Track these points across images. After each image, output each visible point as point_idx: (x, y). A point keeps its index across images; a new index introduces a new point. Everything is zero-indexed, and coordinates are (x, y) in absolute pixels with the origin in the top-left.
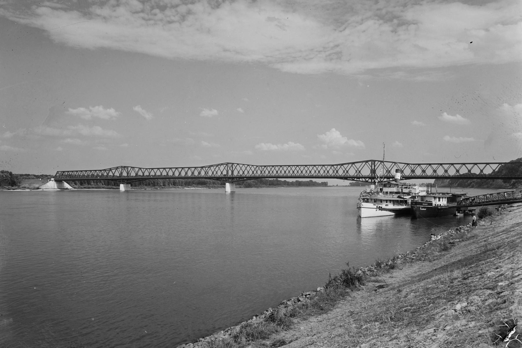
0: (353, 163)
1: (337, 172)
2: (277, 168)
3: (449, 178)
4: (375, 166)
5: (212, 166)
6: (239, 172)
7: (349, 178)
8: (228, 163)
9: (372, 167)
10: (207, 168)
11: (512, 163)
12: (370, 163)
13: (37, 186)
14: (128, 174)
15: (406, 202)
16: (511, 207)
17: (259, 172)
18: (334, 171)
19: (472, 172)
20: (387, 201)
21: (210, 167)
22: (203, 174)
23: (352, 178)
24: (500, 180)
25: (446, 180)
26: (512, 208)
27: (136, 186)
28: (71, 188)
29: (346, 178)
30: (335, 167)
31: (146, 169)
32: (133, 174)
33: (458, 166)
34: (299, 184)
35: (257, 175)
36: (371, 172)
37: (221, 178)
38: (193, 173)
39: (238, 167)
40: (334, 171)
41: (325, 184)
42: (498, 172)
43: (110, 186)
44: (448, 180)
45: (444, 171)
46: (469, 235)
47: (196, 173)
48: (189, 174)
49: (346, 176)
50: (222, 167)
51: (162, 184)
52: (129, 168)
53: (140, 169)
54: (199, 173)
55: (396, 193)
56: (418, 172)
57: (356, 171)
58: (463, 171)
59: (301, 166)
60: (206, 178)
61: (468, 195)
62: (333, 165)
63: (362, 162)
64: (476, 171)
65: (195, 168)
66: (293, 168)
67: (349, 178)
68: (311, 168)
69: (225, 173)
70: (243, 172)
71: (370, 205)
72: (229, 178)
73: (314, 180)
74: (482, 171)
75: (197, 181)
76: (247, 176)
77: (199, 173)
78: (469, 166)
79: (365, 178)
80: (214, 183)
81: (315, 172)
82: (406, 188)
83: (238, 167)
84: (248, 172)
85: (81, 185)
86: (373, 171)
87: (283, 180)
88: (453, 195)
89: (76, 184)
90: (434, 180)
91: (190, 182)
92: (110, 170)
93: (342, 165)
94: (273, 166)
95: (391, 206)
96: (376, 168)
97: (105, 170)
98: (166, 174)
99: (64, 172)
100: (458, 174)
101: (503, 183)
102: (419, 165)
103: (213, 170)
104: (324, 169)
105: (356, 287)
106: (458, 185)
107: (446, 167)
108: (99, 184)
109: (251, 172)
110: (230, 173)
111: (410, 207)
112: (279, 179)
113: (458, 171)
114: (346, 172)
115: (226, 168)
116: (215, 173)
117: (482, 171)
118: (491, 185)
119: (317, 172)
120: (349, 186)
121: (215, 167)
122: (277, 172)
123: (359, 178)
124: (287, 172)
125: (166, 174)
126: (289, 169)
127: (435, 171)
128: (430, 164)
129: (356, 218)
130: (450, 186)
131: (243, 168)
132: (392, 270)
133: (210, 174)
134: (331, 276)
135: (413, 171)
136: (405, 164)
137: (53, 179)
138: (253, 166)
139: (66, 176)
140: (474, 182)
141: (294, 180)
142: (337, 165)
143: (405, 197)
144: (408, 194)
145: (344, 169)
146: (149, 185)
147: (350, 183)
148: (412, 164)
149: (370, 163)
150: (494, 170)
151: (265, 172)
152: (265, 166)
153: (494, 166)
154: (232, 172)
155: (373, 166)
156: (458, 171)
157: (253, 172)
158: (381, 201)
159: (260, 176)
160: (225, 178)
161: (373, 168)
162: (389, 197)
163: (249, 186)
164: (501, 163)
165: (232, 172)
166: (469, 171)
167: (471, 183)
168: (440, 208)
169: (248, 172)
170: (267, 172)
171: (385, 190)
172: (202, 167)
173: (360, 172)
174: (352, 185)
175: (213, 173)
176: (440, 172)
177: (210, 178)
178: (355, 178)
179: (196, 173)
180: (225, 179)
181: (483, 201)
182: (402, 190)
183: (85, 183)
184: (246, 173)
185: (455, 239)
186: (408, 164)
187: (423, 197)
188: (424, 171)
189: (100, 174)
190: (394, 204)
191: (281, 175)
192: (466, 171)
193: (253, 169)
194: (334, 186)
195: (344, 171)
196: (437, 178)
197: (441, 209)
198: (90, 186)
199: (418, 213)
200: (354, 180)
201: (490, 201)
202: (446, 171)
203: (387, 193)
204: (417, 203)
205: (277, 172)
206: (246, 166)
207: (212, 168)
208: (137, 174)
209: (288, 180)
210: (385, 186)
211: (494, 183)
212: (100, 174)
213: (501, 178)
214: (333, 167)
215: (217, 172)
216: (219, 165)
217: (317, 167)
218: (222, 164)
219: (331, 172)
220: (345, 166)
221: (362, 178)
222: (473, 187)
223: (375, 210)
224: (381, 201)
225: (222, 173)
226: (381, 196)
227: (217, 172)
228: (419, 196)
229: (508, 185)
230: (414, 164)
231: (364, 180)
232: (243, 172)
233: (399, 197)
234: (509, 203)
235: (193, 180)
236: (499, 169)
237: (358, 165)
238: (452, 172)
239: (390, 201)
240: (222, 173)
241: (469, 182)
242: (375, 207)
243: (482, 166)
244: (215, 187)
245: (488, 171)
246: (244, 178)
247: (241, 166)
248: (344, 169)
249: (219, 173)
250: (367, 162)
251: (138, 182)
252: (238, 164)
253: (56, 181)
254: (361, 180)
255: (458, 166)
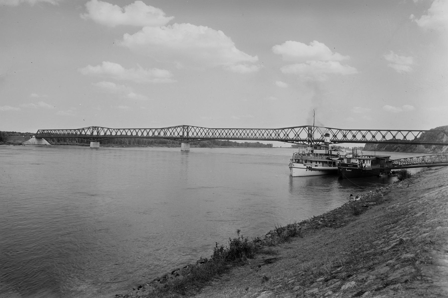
0: (293, 128)
1: (279, 135)
2: (233, 131)
3: (376, 142)
4: (311, 131)
5: (170, 128)
6: (193, 134)
7: (289, 140)
8: (184, 126)
9: (309, 131)
10: (166, 130)
11: (431, 131)
12: (307, 128)
13: (20, 142)
14: (98, 133)
15: (334, 164)
16: (430, 170)
17: (211, 134)
18: (276, 135)
19: (397, 138)
20: (316, 162)
21: (168, 128)
22: (162, 134)
23: (292, 141)
24: (422, 146)
25: (375, 144)
26: (431, 171)
27: (105, 144)
28: (49, 144)
29: (286, 141)
30: (277, 131)
31: (114, 129)
32: (102, 134)
33: (384, 133)
34: (247, 145)
35: (209, 136)
36: (308, 136)
37: (178, 138)
38: (153, 134)
39: (193, 130)
40: (276, 135)
41: (270, 146)
42: (420, 138)
43: (82, 144)
44: (377, 145)
45: (352, 136)
46: (384, 198)
47: (156, 134)
48: (151, 134)
49: (297, 139)
50: (179, 129)
51: (128, 143)
52: (99, 128)
53: (109, 129)
54: (159, 134)
55: (326, 155)
56: (349, 137)
57: (295, 135)
58: (389, 137)
59: (255, 129)
60: (164, 138)
61: (391, 158)
62: (275, 130)
63: (301, 127)
64: (400, 137)
65: (156, 129)
66: (241, 131)
67: (289, 140)
68: (256, 131)
69: (181, 134)
70: (197, 134)
71: (301, 166)
72: (185, 138)
73: (261, 142)
74: (405, 137)
75: (158, 140)
76: (200, 137)
77: (159, 134)
78: (394, 133)
79: (303, 141)
80: (173, 143)
81: (260, 134)
82: (335, 150)
83: (193, 130)
84: (201, 134)
85: (58, 142)
86: (310, 135)
87: (234, 141)
88: (376, 158)
89: (53, 141)
90: (365, 144)
91: (152, 142)
92: (83, 129)
93: (283, 129)
94: (223, 129)
95: (320, 167)
96: (312, 132)
97: (79, 130)
98: (125, 134)
99: (44, 130)
100: (384, 140)
101: (424, 149)
102: (350, 130)
103: (171, 131)
104: (268, 132)
105: (241, 260)
106: (386, 149)
107: (373, 133)
108: (73, 141)
109: (203, 134)
110: (185, 134)
111: (337, 168)
112: (230, 141)
113: (384, 137)
114: (286, 135)
115: (182, 130)
116: (172, 134)
117: (405, 137)
118: (414, 149)
119: (261, 135)
120: (291, 148)
121: (173, 129)
122: (226, 134)
123: (298, 141)
124: (235, 134)
125: (125, 134)
126: (244, 132)
127: (364, 137)
128: (360, 131)
129: (288, 178)
130: (379, 150)
131: (197, 130)
132: (291, 238)
133: (168, 134)
134: (218, 246)
135: (345, 136)
136: (338, 129)
137: (34, 136)
138: (205, 128)
139: (46, 134)
140: (399, 147)
141: (243, 141)
142: (279, 129)
143: (333, 159)
144: (337, 156)
145: (285, 133)
146: (117, 143)
147: (292, 146)
148: (344, 130)
149: (307, 128)
150: (416, 137)
151: (216, 134)
152: (216, 129)
153: (416, 133)
154: (188, 133)
155: (310, 131)
156: (384, 137)
157: (206, 134)
158: (311, 162)
159: (212, 137)
160: (181, 138)
161: (310, 132)
162: (319, 159)
163: (203, 146)
164: (422, 131)
165: (188, 133)
166: (394, 137)
167: (397, 148)
168: (364, 169)
169: (201, 134)
170: (218, 134)
171: (316, 151)
172: (162, 129)
173: (298, 135)
174: (293, 147)
175: (171, 134)
176: (369, 137)
177: (168, 138)
178: (294, 140)
179: (140, 134)
180: (180, 140)
181: (404, 164)
182: (331, 152)
183: (62, 140)
184: (199, 134)
185: (370, 202)
186: (340, 130)
187: (349, 159)
188: (354, 136)
189: (74, 133)
190: (323, 165)
191: (230, 137)
192: (391, 138)
193: (205, 131)
194: (278, 147)
195: (285, 135)
196: (367, 142)
197: (365, 171)
198: (66, 143)
199: (343, 174)
200: (293, 143)
201: (410, 165)
202: (374, 137)
203: (317, 154)
204: (344, 165)
205: (226, 134)
206: (203, 129)
207: (170, 129)
208: (105, 134)
209: (238, 141)
210: (316, 148)
211: (417, 148)
212: (74, 133)
213: (423, 144)
214: (275, 131)
215: (174, 134)
216: (176, 127)
217: (261, 130)
218: (179, 126)
219: (273, 135)
220: (286, 130)
221: (301, 141)
222: (398, 151)
223: (306, 170)
224: (311, 162)
225: (178, 134)
226: (311, 157)
227: (174, 134)
228: (346, 158)
229: (429, 150)
230: (345, 130)
231: (302, 142)
232: (197, 134)
233: (328, 159)
234: (428, 167)
235: (155, 139)
236: (421, 136)
237: (296, 130)
238: (379, 138)
239: (320, 162)
240: (178, 134)
241: (395, 146)
242: (306, 167)
243: (405, 133)
244: (173, 147)
245: (410, 137)
246: (197, 138)
247: (195, 128)
248: (285, 133)
249: (176, 134)
250: (304, 127)
251: (106, 141)
252: (193, 127)
253: (36, 138)
254: (299, 142)
255: (384, 133)
